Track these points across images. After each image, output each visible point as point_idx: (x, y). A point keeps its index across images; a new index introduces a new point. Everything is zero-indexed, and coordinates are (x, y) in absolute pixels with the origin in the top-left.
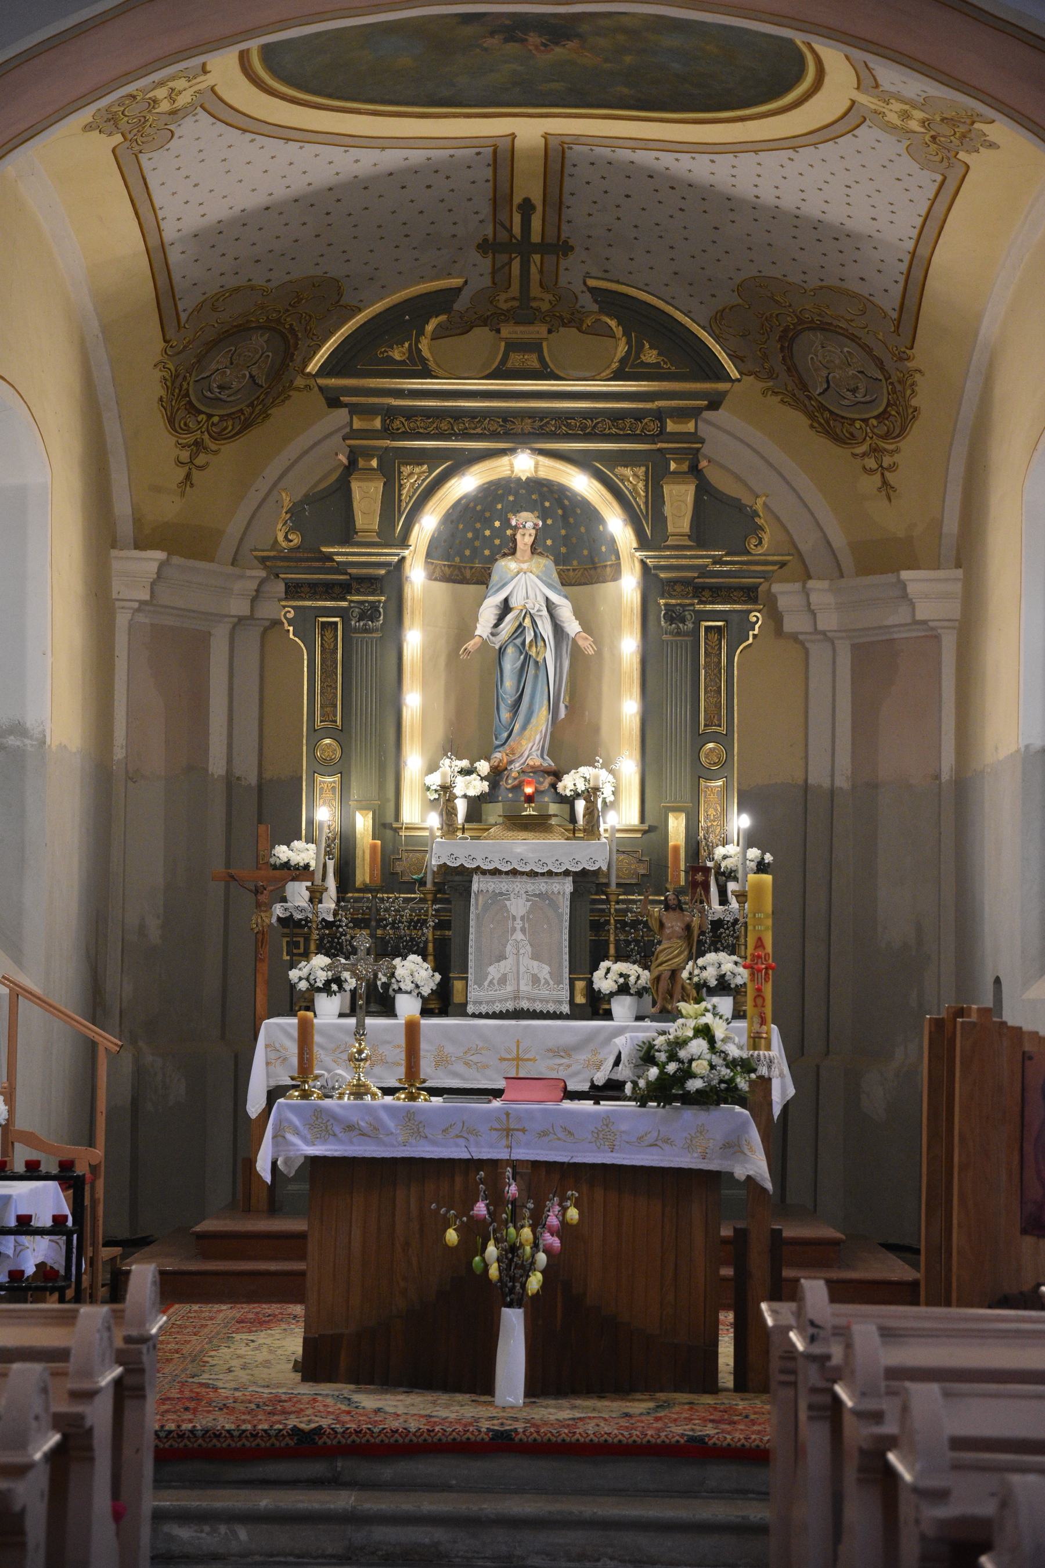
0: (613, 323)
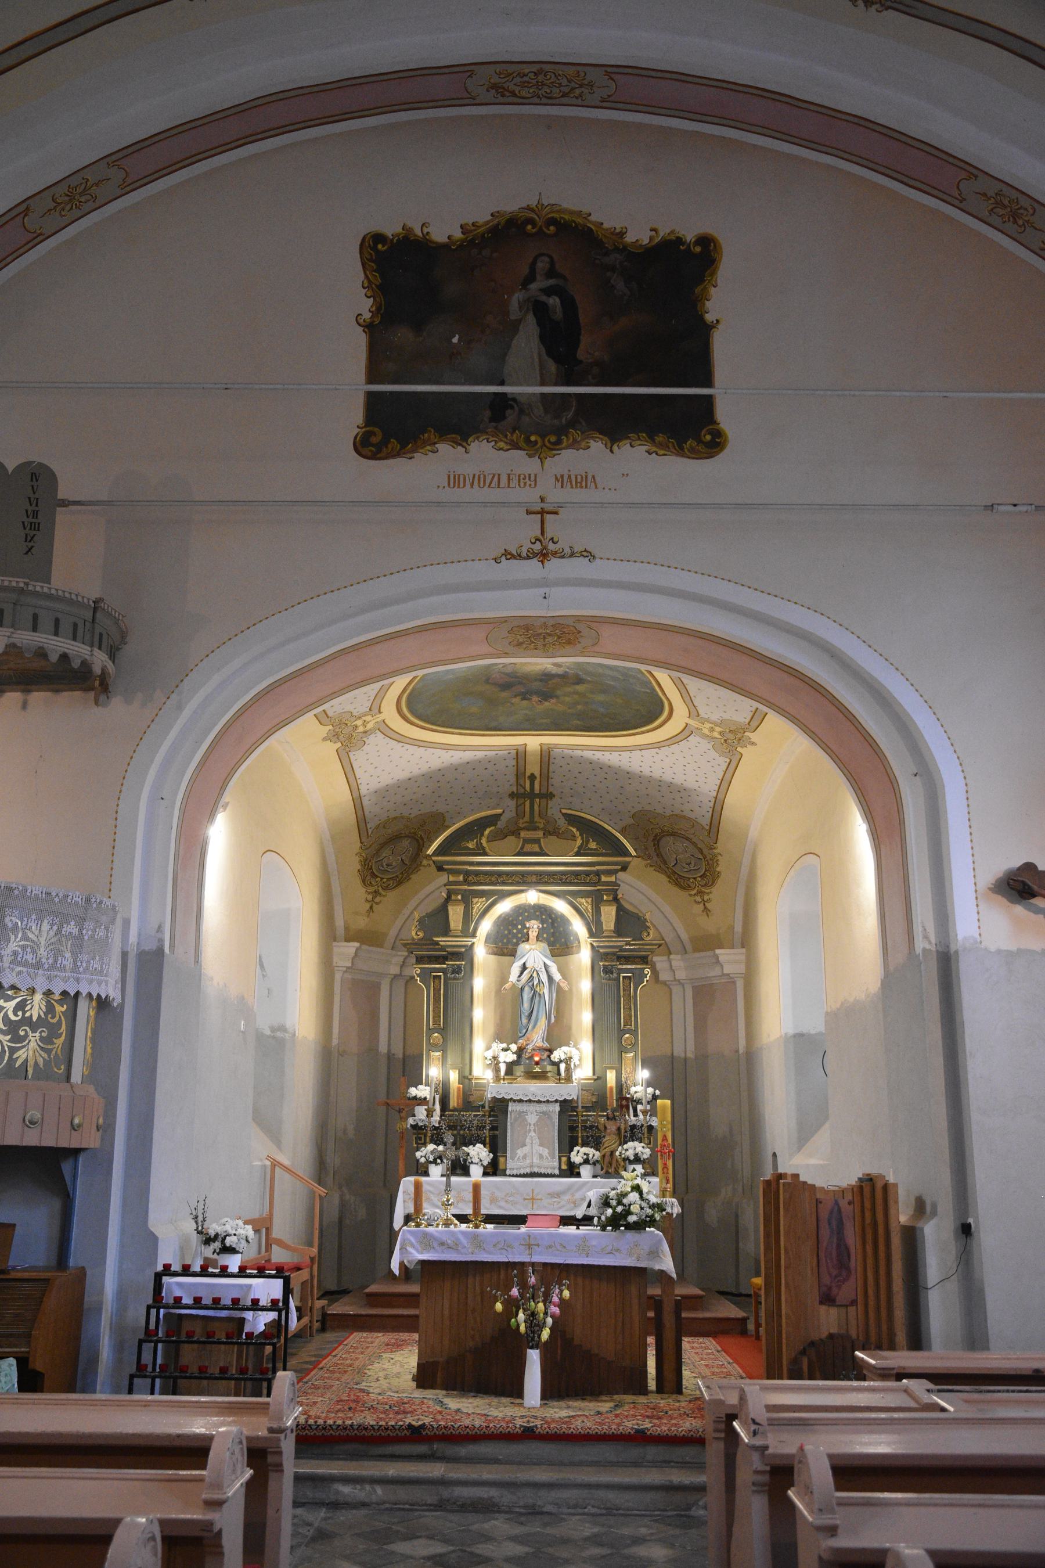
0: (574, 830)
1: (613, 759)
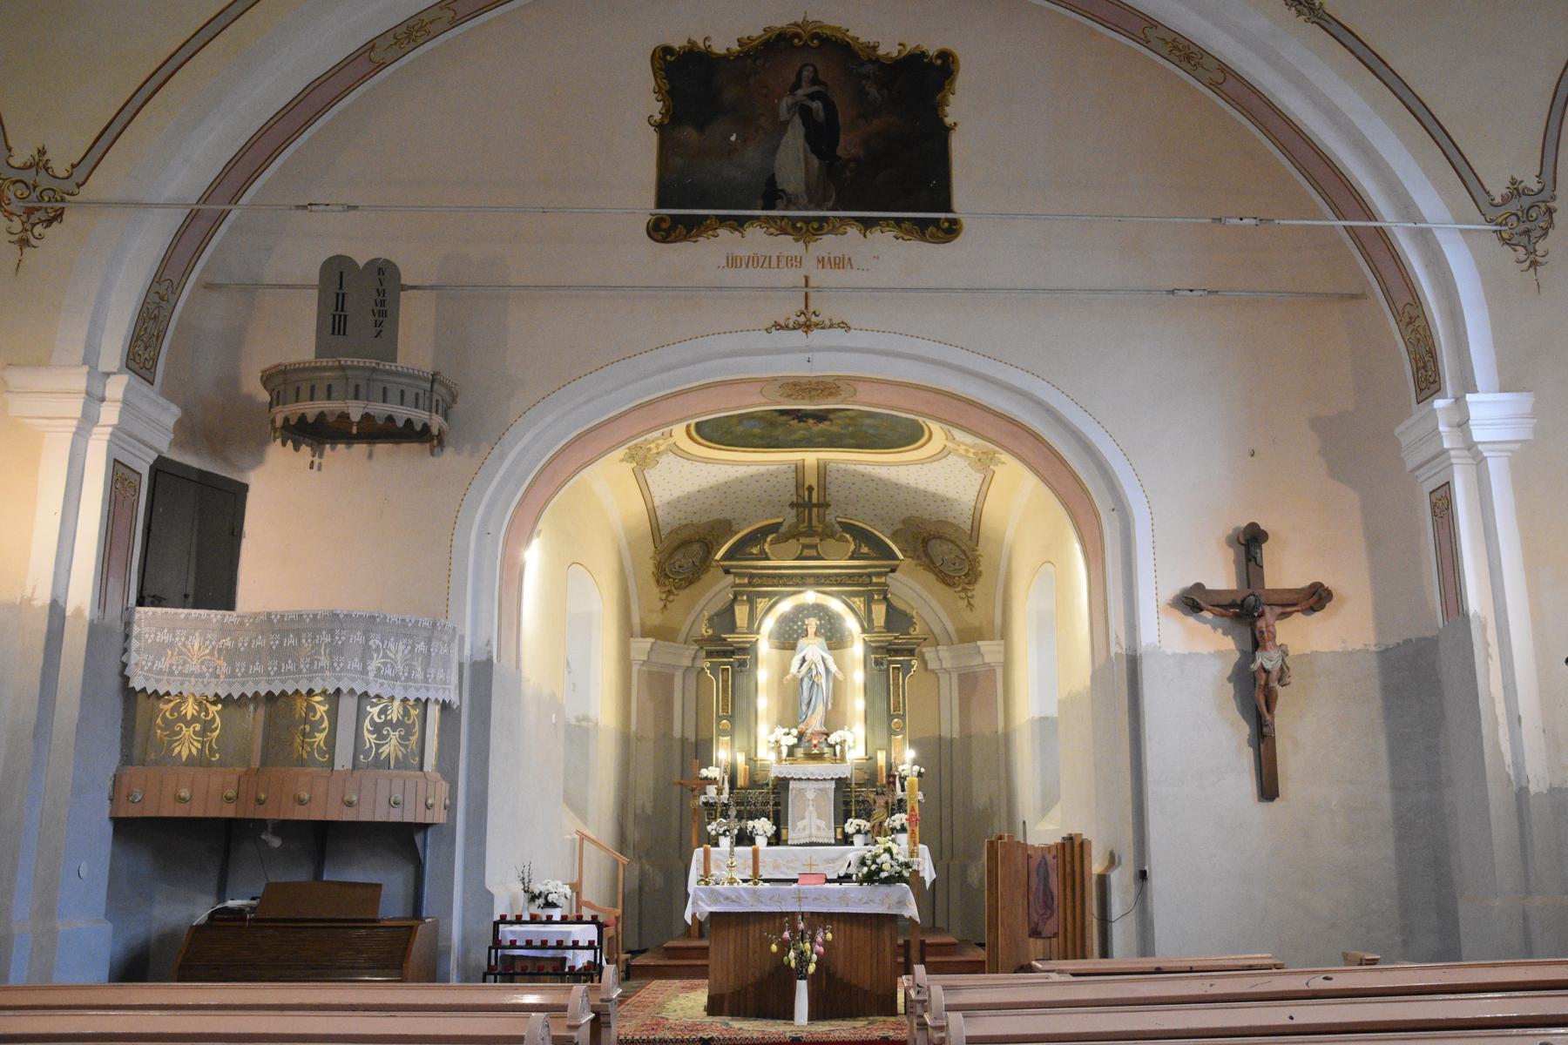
1: (883, 472)
